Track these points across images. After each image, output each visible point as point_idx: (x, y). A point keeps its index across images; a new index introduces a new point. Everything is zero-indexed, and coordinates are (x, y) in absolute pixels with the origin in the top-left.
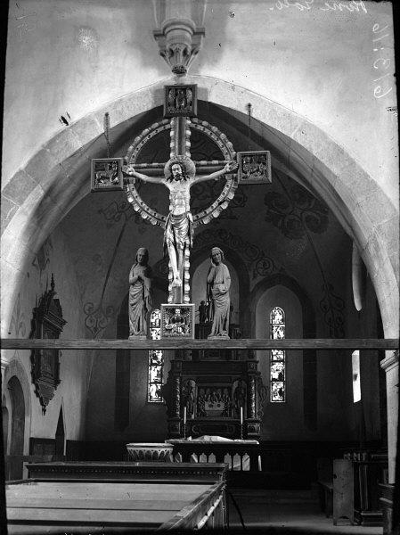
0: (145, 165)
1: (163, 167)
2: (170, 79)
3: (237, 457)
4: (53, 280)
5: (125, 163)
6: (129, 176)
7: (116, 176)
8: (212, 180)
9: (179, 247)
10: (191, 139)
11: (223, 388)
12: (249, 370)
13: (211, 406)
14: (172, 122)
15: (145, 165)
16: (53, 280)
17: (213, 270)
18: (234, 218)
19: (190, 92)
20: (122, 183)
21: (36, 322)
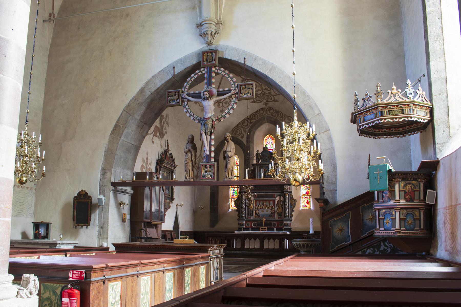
2: (204, 47)
3: (272, 240)
4: (168, 142)
5: (183, 92)
6: (184, 98)
7: (178, 98)
9: (208, 134)
11: (270, 201)
12: (285, 190)
13: (263, 211)
14: (206, 70)
16: (168, 142)
19: (214, 54)
20: (181, 102)
21: (158, 167)
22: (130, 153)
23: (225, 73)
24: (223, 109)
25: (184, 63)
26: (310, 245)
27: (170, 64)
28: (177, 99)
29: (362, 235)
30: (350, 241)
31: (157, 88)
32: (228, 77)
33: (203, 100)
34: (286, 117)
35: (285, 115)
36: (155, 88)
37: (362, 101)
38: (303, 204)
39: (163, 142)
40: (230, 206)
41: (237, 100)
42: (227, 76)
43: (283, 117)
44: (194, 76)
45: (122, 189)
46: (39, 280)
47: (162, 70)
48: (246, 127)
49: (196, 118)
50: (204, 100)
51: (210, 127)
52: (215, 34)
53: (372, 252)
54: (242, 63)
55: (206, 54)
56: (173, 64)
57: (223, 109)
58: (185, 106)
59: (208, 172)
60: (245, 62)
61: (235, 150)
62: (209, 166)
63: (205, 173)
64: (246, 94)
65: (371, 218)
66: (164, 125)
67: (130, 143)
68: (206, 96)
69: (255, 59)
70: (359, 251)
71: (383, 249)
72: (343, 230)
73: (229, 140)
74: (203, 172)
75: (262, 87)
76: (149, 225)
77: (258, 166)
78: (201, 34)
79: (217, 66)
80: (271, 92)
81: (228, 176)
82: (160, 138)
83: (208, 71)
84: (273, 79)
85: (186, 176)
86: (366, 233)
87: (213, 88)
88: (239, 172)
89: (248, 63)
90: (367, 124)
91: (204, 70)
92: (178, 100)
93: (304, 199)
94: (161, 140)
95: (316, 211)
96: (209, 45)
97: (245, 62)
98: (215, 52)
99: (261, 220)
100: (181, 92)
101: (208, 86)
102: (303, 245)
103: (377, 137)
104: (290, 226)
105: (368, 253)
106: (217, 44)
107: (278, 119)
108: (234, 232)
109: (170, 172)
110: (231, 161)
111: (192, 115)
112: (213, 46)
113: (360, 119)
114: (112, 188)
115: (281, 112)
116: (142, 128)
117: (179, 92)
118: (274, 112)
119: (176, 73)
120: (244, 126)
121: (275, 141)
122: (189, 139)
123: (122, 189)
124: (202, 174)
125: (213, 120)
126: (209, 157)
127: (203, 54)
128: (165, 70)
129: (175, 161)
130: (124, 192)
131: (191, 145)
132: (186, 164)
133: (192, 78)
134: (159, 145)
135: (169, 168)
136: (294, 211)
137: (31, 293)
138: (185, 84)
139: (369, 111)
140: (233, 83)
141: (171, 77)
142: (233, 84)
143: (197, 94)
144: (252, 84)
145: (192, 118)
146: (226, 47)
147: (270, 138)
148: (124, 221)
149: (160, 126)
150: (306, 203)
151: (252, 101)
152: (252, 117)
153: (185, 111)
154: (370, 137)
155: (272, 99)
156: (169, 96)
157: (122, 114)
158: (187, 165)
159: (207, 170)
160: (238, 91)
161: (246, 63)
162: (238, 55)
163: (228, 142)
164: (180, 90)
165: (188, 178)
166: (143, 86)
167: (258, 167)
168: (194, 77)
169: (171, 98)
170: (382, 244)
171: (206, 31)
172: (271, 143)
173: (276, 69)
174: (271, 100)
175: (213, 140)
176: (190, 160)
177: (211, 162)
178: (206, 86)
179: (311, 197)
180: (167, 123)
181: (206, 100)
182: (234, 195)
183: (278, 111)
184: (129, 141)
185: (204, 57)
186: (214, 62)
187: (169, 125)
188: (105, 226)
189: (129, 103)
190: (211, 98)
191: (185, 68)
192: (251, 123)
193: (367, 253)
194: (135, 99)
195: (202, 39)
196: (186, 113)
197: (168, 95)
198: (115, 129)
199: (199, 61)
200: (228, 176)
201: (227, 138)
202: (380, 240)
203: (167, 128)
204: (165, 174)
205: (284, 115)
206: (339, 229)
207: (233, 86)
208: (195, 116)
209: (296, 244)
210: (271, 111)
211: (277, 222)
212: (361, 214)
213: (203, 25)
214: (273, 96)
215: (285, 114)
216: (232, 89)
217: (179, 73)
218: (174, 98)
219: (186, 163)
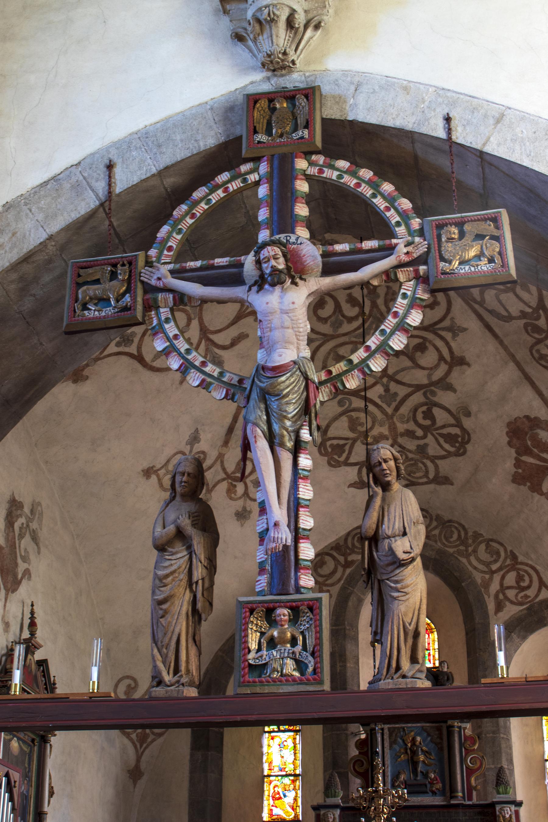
0: (198, 264)
1: (242, 265)
4: (32, 613)
8: (364, 284)
9: (282, 445)
10: (309, 199)
14: (264, 168)
15: (198, 264)
16: (32, 613)
17: (378, 502)
18: (446, 481)
19: (302, 101)
20: (139, 308)
23: (358, 178)
24: (244, 509)
25: (159, 146)
27: (93, 154)
28: (123, 295)
31: (25, 251)
33: (255, 288)
34: (481, 542)
35: (477, 535)
36: (15, 251)
41: (424, 291)
43: (470, 541)
48: (329, 582)
49: (219, 379)
51: (292, 410)
52: (306, 27)
55: (263, 104)
56: (109, 152)
57: (244, 509)
58: (160, 324)
59: (283, 642)
60: (449, 131)
61: (422, 528)
62: (286, 611)
63: (264, 652)
66: (23, 542)
68: (273, 262)
69: (499, 120)
73: (392, 478)
74: (253, 646)
75: (394, 424)
77: (386, 727)
79: (318, 153)
80: (426, 445)
81: (394, 664)
83: (276, 171)
85: (155, 667)
88: (299, 756)
91: (255, 170)
94: (6, 599)
96: (278, 73)
97: (449, 131)
98: (307, 96)
100: (141, 261)
107: (451, 550)
109: (33, 741)
110: (408, 581)
111: (197, 363)
115: (460, 524)
117: (130, 263)
118: (434, 524)
119: (118, 189)
120: (322, 576)
122: (178, 478)
124: (251, 656)
125: (307, 379)
128: (69, 176)
131: (187, 507)
132: (161, 603)
133: (196, 203)
138: (165, 229)
140: (398, 219)
141: (93, 206)
142: (398, 224)
144: (495, 220)
145: (194, 378)
146: (356, 79)
149: (7, 539)
151: (355, 483)
152: (353, 545)
155: (427, 472)
156: (80, 280)
158: (166, 612)
159: (276, 634)
160: (429, 248)
161: (454, 138)
162: (417, 106)
164: (141, 255)
165: (167, 678)
167: (386, 731)
168: (205, 198)
174: (425, 480)
176: (184, 583)
177: (298, 589)
180: (35, 539)
181: (273, 285)
183: (450, 521)
186: (306, 132)
187: (39, 548)
190: (298, 280)
191: (162, 166)
192: (347, 564)
195: (246, 55)
197: (79, 276)
199: (228, 136)
200: (394, 664)
201: (384, 466)
203: (32, 557)
204: (15, 744)
205: (470, 534)
214: (433, 459)
215: (475, 532)
217: (133, 190)
218: (104, 290)
219: (160, 597)
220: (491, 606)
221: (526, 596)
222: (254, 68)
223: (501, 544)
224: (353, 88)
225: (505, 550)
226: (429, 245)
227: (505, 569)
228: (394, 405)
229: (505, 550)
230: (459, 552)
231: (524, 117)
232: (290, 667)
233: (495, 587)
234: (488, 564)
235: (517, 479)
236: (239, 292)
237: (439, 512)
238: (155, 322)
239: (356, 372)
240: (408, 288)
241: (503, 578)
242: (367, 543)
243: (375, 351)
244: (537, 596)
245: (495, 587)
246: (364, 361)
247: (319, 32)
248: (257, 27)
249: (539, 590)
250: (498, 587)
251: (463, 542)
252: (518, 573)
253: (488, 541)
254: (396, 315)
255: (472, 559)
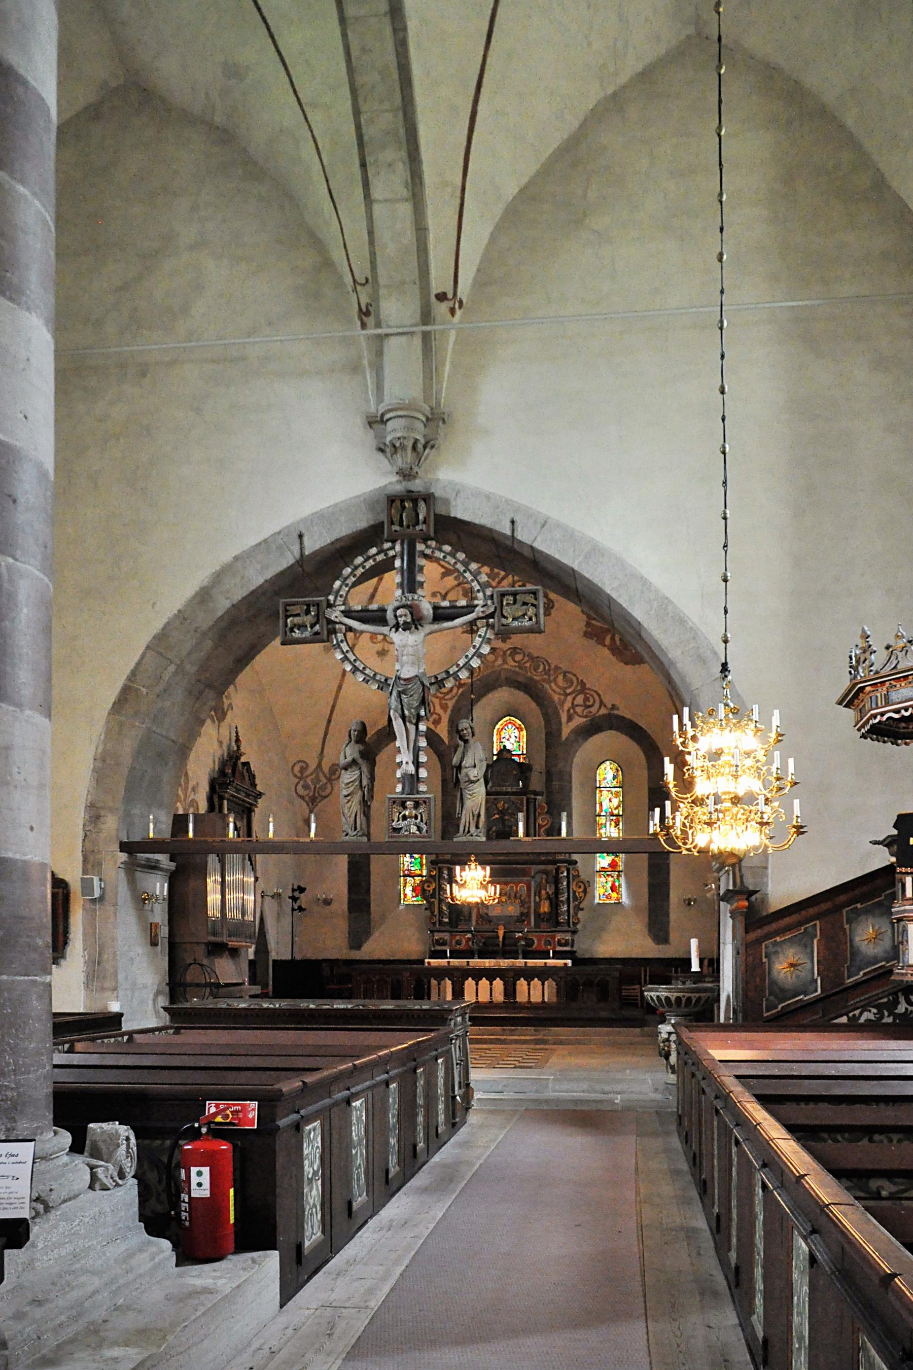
4: (237, 733)
14: (398, 547)
16: (237, 733)
20: (325, 632)
21: (216, 800)
22: (166, 764)
24: (383, 650)
26: (696, 1001)
27: (288, 527)
29: (848, 979)
30: (816, 991)
32: (465, 571)
33: (394, 630)
37: (885, 654)
38: (602, 891)
39: (225, 732)
40: (402, 896)
42: (462, 569)
43: (552, 672)
44: (364, 562)
45: (148, 859)
46: (137, 1138)
47: (265, 541)
50: (397, 630)
52: (425, 447)
53: (873, 1019)
54: (504, 535)
55: (398, 503)
57: (383, 650)
60: (513, 530)
64: (519, 618)
65: (874, 938)
67: (167, 738)
70: (841, 1016)
71: (903, 1010)
72: (799, 965)
74: (396, 819)
76: (217, 949)
78: (383, 447)
79: (432, 539)
81: (467, 830)
82: (216, 721)
84: (596, 580)
86: (858, 974)
87: (421, 598)
89: (522, 535)
90: (897, 711)
91: (393, 548)
92: (317, 627)
93: (603, 879)
95: (636, 908)
97: (513, 530)
98: (425, 500)
99: (493, 932)
101: (406, 591)
102: (678, 999)
103: (900, 741)
104: (572, 946)
105: (866, 1021)
106: (430, 476)
108: (422, 962)
111: (361, 669)
112: (417, 481)
113: (873, 698)
114: (123, 857)
116: (198, 699)
118: (526, 659)
121: (524, 733)
122: (352, 732)
123: (148, 858)
124: (394, 824)
126: (412, 780)
127: (390, 503)
129: (257, 781)
130: (153, 867)
133: (356, 568)
134: (215, 740)
135: (243, 801)
136: (582, 909)
137: (122, 1175)
138: (337, 584)
139: (906, 677)
140: (479, 588)
142: (478, 591)
143: (371, 614)
147: (510, 726)
148: (154, 943)
150: (609, 889)
153: (339, 656)
154: (884, 742)
156: (289, 613)
157: (143, 657)
161: (515, 535)
163: (466, 742)
166: (205, 583)
169: (297, 620)
170: (902, 999)
171: (399, 438)
172: (512, 740)
173: (603, 555)
175: (422, 736)
178: (399, 592)
179: (622, 874)
182: (412, 869)
183: (538, 657)
184: (164, 733)
185: (393, 511)
188: (106, 957)
189: (163, 629)
190: (419, 627)
193: (862, 1020)
194: (182, 617)
196: (343, 662)
198: (126, 699)
200: (467, 830)
202: (895, 990)
205: (553, 667)
206: (787, 962)
207: (480, 595)
208: (367, 671)
209: (658, 997)
210: (518, 657)
211: (537, 936)
212: (847, 926)
213: (388, 420)
216: (476, 602)
217: (315, 553)
220: (564, 718)
221: (591, 712)
222: (391, 473)
223: (575, 675)
224: (454, 494)
225: (577, 679)
226: (496, 607)
227: (578, 693)
228: (497, 580)
229: (577, 679)
230: (544, 680)
231: (558, 525)
232: (414, 829)
233: (568, 705)
234: (564, 689)
235: (587, 635)
236: (385, 630)
237: (532, 651)
238: (335, 642)
239: (451, 678)
240: (482, 632)
241: (574, 699)
242: (455, 770)
243: (462, 668)
244: (598, 712)
245: (568, 705)
246: (455, 673)
247: (434, 450)
248: (393, 449)
249: (600, 708)
250: (570, 705)
251: (547, 672)
252: (585, 696)
253: (565, 673)
254: (474, 647)
255: (553, 685)
